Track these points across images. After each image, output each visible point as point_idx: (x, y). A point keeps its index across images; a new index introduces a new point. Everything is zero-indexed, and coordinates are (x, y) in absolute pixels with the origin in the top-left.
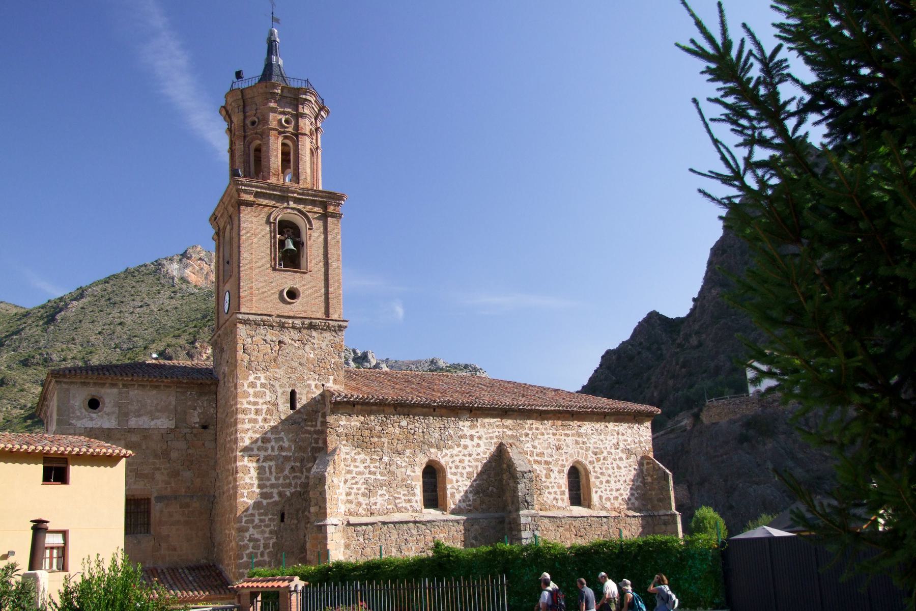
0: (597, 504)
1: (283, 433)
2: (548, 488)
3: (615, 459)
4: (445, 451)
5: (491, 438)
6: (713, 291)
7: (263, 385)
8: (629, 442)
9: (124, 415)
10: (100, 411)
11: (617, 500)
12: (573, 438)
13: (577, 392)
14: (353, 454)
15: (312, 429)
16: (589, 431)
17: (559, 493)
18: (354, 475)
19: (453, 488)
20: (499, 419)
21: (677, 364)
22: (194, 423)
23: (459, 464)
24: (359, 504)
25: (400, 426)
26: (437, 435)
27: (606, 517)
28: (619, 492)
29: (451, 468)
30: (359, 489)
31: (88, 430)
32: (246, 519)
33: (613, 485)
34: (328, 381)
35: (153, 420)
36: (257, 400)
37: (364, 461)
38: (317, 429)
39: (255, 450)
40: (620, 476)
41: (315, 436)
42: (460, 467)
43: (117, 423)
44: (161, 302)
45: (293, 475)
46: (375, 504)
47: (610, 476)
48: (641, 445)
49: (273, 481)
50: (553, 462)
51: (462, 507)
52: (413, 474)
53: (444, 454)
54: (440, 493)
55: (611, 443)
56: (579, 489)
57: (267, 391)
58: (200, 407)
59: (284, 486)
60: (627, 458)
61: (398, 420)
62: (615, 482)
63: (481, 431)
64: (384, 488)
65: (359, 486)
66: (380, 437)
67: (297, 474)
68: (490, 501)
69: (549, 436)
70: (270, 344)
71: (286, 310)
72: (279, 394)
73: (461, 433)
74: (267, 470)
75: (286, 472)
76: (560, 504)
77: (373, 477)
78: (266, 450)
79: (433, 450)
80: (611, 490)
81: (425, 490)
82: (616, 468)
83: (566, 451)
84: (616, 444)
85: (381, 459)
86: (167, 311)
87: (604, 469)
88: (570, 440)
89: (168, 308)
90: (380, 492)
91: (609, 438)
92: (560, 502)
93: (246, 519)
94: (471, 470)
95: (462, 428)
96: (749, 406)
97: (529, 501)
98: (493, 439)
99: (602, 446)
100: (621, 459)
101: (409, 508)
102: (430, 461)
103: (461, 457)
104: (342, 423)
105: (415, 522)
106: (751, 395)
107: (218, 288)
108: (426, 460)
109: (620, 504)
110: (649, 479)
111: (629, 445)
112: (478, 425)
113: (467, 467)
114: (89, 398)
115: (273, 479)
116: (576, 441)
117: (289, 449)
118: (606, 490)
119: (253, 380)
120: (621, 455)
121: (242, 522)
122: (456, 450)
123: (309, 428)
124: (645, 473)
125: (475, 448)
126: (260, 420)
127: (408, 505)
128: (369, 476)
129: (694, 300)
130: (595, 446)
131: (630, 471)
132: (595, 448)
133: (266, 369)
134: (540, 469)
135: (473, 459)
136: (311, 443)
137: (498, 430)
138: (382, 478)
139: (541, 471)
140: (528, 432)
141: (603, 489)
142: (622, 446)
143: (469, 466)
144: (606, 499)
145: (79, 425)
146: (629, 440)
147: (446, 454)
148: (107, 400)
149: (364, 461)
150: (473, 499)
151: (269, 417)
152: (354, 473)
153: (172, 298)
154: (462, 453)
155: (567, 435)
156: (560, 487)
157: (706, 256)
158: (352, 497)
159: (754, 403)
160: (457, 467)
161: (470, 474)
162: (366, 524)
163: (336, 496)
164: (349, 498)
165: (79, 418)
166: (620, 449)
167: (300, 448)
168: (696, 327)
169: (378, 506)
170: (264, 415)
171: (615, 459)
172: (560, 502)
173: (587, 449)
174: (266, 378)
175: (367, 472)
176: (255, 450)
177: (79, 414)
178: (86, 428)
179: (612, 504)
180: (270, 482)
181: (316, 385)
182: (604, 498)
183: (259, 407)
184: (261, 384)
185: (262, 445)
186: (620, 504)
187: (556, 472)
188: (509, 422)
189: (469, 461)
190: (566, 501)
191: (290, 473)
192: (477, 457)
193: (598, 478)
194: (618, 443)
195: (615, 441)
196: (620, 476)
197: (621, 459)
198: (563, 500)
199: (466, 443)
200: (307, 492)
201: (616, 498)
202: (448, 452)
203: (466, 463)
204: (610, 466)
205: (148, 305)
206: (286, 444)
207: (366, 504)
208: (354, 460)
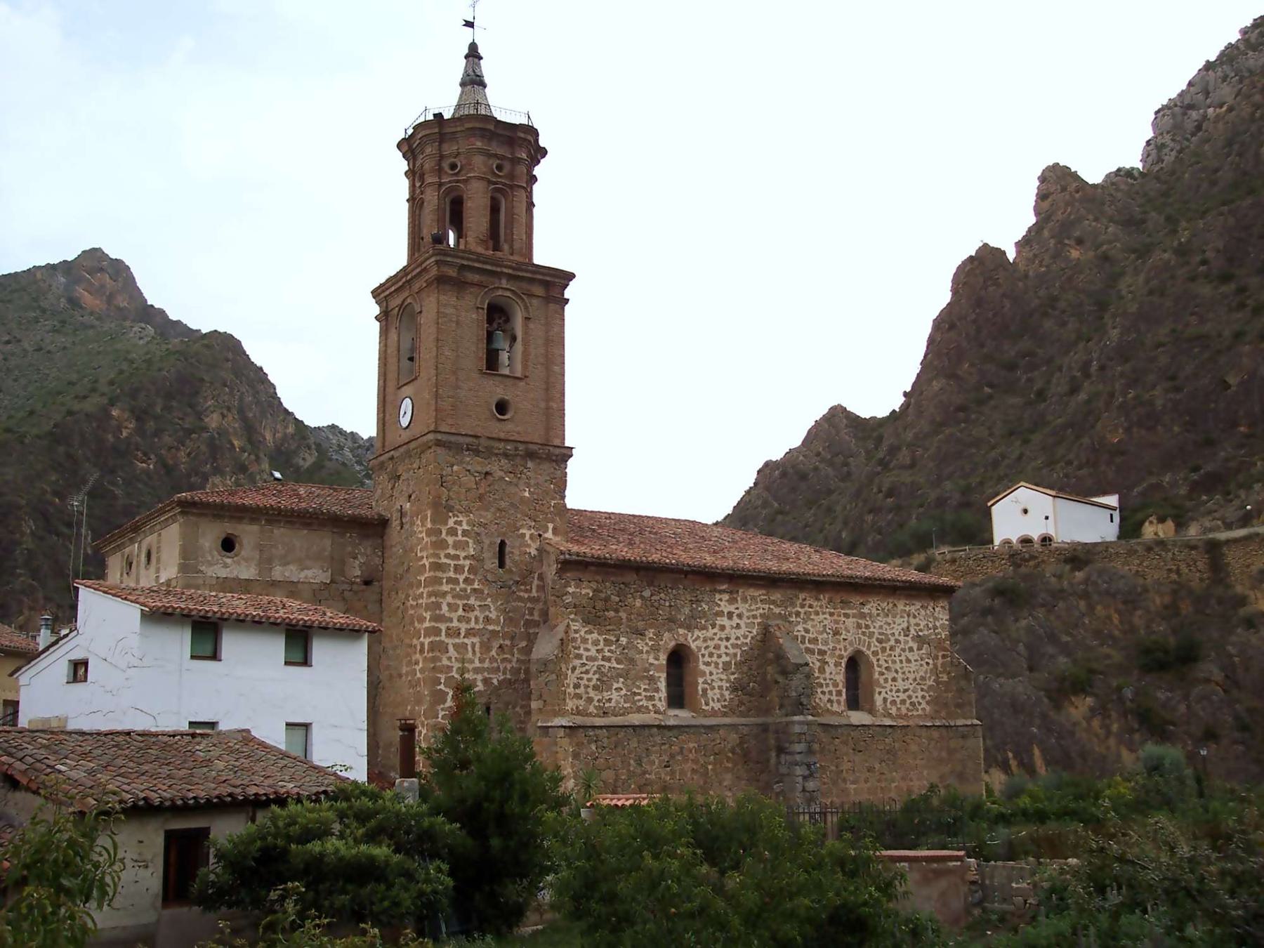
0: (880, 708)
1: (489, 600)
2: (821, 686)
3: (904, 650)
4: (697, 633)
5: (755, 617)
6: (934, 383)
7: (465, 533)
8: (922, 627)
9: (266, 563)
10: (236, 556)
11: (905, 704)
12: (855, 620)
13: (716, 524)
14: (582, 633)
15: (526, 596)
16: (874, 612)
17: (834, 693)
18: (585, 661)
19: (705, 682)
20: (764, 592)
21: (880, 491)
22: (355, 577)
23: (714, 651)
24: (590, 700)
25: (642, 597)
26: (687, 610)
27: (891, 726)
28: (907, 694)
29: (703, 656)
30: (589, 680)
31: (221, 580)
32: (444, 713)
33: (901, 684)
34: (546, 531)
35: (302, 570)
36: (458, 553)
37: (596, 643)
38: (532, 595)
39: (455, 620)
40: (910, 672)
41: (529, 605)
42: (715, 655)
43: (257, 572)
44: (39, 337)
45: (501, 657)
46: (609, 701)
47: (897, 672)
48: (936, 631)
49: (477, 664)
50: (829, 652)
51: (716, 709)
52: (656, 662)
53: (695, 636)
54: (687, 690)
55: (900, 627)
56: (856, 688)
57: (471, 541)
58: (362, 554)
59: (489, 670)
60: (919, 649)
61: (640, 589)
62: (903, 680)
63: (743, 608)
64: (621, 680)
65: (590, 676)
66: (617, 611)
67: (506, 656)
68: (750, 702)
69: (825, 616)
70: (475, 477)
71: (497, 429)
72: (486, 547)
73: (717, 608)
74: (470, 649)
75: (493, 653)
76: (835, 708)
77: (607, 664)
78: (468, 621)
79: (681, 631)
80: (898, 691)
81: (669, 685)
82: (904, 661)
83: (845, 637)
84: (905, 629)
85: (618, 640)
86: (49, 352)
87: (890, 662)
88: (850, 622)
89: (51, 348)
90: (615, 685)
91: (898, 620)
92: (835, 705)
93: (444, 713)
94: (728, 659)
95: (719, 602)
96: (997, 563)
97: (805, 703)
98: (757, 618)
99: (889, 632)
100: (911, 649)
101: (651, 707)
102: (678, 645)
103: (716, 641)
104: (570, 590)
105: (659, 727)
106: (996, 548)
107: (384, 390)
108: (673, 644)
109: (908, 709)
110: (945, 678)
111: (921, 630)
112: (739, 599)
113: (724, 656)
114: (224, 536)
115: (477, 661)
116: (858, 623)
117: (497, 622)
118: (891, 691)
119: (452, 525)
120: (911, 644)
121: (438, 718)
122: (711, 632)
123: (522, 594)
124: (940, 669)
125: (734, 630)
126: (461, 581)
127: (650, 704)
128: (602, 663)
129: (408, 200)
130: (880, 631)
131: (921, 665)
132: (880, 634)
133: (468, 511)
134: (813, 661)
135: (732, 645)
136: (524, 614)
137: (764, 606)
138: (619, 666)
139: (813, 663)
140: (800, 610)
141: (888, 689)
142: (913, 632)
143: (726, 654)
144: (891, 703)
145: (209, 574)
146: (923, 623)
147: (698, 637)
148: (245, 542)
149: (596, 643)
150: (730, 699)
151: (472, 577)
152: (584, 657)
153: (57, 331)
154: (718, 636)
155: (847, 616)
156: (835, 685)
157: (927, 329)
158: (581, 690)
159: (1003, 559)
160: (711, 655)
161: (727, 666)
162: (601, 727)
163: (563, 689)
164: (577, 691)
165: (210, 564)
166: (911, 636)
167: (511, 619)
168: (909, 436)
169: (613, 704)
170: (466, 574)
171: (904, 650)
172: (835, 705)
173: (871, 635)
174: (468, 524)
175: (600, 657)
176: (455, 620)
177: (210, 559)
178: (218, 578)
179: (899, 709)
180: (473, 665)
181: (531, 535)
182: (889, 701)
183: (461, 562)
184: (464, 531)
185: (463, 614)
186: (908, 709)
187: (832, 665)
188: (777, 596)
189: (726, 647)
190: (842, 704)
191: (498, 655)
192: (736, 642)
193: (883, 674)
194: (908, 628)
195: (905, 625)
196: (910, 672)
197: (911, 649)
198: (839, 702)
199: (722, 623)
200: (527, 681)
201: (903, 702)
202: (702, 634)
203: (723, 650)
204: (897, 659)
205: (19, 341)
206: (493, 615)
207: (599, 701)
208: (585, 641)
